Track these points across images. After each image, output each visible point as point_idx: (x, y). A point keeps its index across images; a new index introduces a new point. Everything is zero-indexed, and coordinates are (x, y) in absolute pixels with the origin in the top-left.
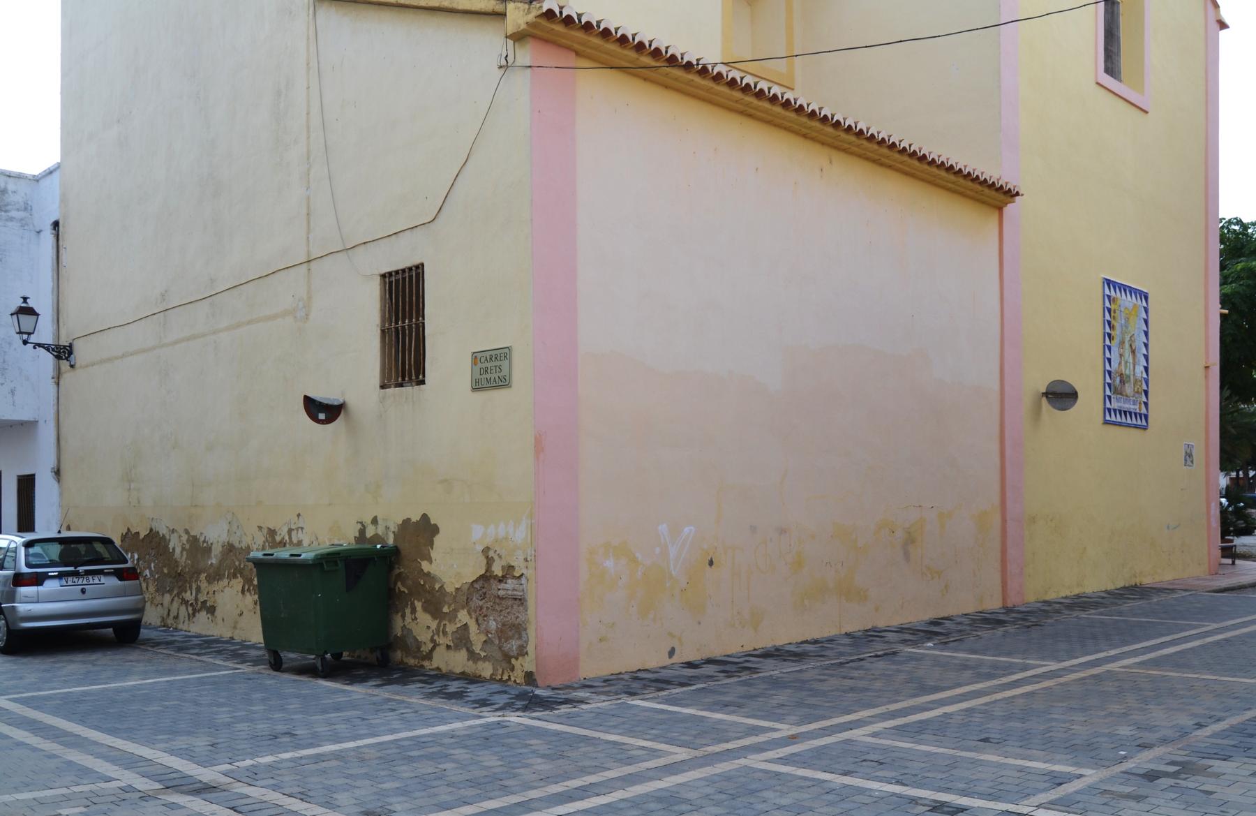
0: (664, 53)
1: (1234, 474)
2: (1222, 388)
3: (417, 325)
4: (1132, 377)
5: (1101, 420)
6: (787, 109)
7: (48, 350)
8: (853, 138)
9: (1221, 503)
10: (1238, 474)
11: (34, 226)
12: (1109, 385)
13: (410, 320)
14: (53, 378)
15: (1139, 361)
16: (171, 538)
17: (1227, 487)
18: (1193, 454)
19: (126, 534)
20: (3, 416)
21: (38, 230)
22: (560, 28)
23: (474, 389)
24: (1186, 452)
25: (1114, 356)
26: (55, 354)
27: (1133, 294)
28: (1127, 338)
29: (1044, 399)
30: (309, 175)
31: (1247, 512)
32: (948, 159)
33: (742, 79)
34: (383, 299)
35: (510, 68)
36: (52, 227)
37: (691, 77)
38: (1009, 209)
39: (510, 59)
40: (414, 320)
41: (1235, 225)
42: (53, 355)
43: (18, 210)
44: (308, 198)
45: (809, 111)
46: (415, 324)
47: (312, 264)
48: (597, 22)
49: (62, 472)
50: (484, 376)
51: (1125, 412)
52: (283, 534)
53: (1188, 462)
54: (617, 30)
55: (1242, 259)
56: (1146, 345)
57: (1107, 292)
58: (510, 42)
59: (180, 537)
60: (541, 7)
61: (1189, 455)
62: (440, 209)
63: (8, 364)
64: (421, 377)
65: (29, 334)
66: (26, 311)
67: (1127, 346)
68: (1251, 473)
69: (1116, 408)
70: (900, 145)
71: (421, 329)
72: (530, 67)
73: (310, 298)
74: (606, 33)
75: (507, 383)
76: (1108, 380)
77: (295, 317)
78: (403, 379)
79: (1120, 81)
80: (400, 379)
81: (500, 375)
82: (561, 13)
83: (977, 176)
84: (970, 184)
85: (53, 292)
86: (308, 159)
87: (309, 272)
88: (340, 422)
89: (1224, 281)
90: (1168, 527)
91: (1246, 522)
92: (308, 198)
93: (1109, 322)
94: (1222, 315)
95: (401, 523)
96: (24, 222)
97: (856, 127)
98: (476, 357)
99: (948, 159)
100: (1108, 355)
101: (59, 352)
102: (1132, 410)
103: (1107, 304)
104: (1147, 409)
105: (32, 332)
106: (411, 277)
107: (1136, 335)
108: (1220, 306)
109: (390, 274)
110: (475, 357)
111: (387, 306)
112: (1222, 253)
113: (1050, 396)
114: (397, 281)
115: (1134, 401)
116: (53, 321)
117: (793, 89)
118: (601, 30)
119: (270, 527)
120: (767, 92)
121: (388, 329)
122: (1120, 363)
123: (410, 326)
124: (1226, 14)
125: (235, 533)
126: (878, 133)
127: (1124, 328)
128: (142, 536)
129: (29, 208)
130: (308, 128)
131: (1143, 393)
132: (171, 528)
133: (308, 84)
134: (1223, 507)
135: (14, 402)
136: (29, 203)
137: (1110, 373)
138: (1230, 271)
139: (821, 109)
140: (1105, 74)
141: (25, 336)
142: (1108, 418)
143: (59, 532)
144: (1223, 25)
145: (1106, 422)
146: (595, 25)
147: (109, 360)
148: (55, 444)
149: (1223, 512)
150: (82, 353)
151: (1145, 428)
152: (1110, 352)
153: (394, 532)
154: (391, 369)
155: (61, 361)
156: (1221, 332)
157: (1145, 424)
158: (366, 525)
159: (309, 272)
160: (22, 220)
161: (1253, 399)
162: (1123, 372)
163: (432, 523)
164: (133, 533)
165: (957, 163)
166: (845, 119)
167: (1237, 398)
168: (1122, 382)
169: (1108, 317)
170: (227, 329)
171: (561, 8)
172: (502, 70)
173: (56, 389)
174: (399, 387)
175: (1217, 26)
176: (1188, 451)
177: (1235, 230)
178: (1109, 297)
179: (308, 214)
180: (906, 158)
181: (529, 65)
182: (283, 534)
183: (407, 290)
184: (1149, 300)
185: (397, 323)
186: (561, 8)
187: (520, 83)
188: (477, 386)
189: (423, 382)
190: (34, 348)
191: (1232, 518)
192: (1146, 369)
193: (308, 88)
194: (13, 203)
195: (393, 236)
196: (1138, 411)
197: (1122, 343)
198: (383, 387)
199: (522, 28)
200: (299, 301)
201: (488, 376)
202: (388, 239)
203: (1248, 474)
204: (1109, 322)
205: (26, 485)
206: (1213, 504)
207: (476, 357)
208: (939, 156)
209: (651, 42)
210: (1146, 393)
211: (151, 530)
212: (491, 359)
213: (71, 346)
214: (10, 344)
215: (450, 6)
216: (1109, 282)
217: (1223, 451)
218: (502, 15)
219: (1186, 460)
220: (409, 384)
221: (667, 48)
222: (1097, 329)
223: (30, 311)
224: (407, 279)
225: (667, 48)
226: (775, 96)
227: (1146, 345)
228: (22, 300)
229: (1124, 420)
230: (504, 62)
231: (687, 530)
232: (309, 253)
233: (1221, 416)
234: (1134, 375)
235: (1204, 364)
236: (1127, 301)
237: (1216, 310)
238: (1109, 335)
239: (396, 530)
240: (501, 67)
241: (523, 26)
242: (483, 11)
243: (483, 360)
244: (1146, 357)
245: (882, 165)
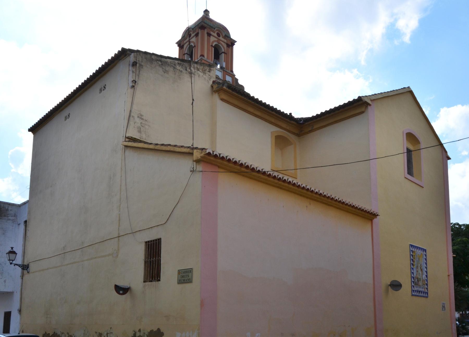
0: (292, 182)
1: (461, 313)
2: (455, 282)
3: (158, 260)
4: (421, 279)
5: (411, 295)
6: (308, 191)
7: (19, 266)
8: (318, 196)
9: (456, 324)
10: (463, 313)
11: (17, 222)
12: (413, 282)
13: (156, 258)
14: (21, 276)
15: (424, 273)
16: (62, 336)
17: (459, 317)
18: (445, 306)
19: (45, 334)
20: (1, 290)
21: (19, 223)
22: (212, 158)
23: (178, 283)
24: (443, 306)
25: (415, 271)
26: (22, 268)
27: (421, 250)
28: (419, 265)
29: (390, 287)
30: (120, 206)
31: (466, 327)
32: (352, 203)
33: (278, 176)
34: (146, 250)
35: (194, 172)
36: (24, 223)
37: (259, 175)
38: (375, 220)
39: (195, 169)
40: (157, 258)
41: (457, 225)
42: (21, 268)
43: (12, 216)
44: (119, 214)
45: (302, 187)
46: (157, 259)
47: (120, 238)
48: (226, 156)
49: (22, 311)
50: (182, 278)
51: (419, 291)
52: (105, 335)
53: (444, 309)
54: (233, 159)
55: (460, 237)
56: (426, 268)
57: (411, 249)
58: (195, 163)
59: (65, 335)
60: (206, 151)
61: (444, 307)
62: (168, 219)
63: (4, 271)
64: (159, 278)
65: (13, 260)
66: (12, 252)
67: (419, 268)
68: (468, 312)
69: (416, 290)
70: (335, 198)
71: (159, 261)
72: (202, 171)
73: (118, 250)
74: (229, 160)
75: (191, 281)
76: (413, 280)
77: (113, 256)
78: (152, 279)
79: (413, 177)
80: (151, 279)
81: (188, 278)
82: (213, 153)
83: (363, 209)
84: (361, 212)
85: (23, 245)
86: (120, 201)
87: (119, 241)
88: (128, 294)
89: (453, 245)
90: (437, 333)
91: (466, 331)
92: (119, 214)
93: (412, 260)
94: (453, 257)
95: (149, 331)
96: (14, 221)
97: (319, 192)
98: (179, 272)
99: (352, 203)
100: (412, 271)
101: (24, 267)
102: (422, 291)
103: (412, 253)
104: (427, 290)
105: (14, 260)
106: (156, 243)
107: (422, 264)
108: (452, 254)
109: (149, 242)
110: (179, 272)
111: (147, 253)
112: (452, 235)
113: (391, 286)
114: (151, 244)
115: (422, 287)
116: (22, 256)
117: (296, 178)
118: (227, 159)
119: (100, 332)
120: (287, 180)
121: (147, 261)
122: (417, 274)
123: (155, 260)
124: (449, 154)
125: (86, 334)
126: (327, 194)
127: (418, 262)
128: (51, 335)
129: (16, 216)
130: (121, 190)
131: (426, 285)
132: (62, 332)
133: (121, 175)
134: (457, 325)
135: (5, 285)
136: (16, 214)
137: (413, 277)
138: (456, 241)
139: (306, 186)
140: (408, 175)
141: (11, 261)
142: (413, 293)
143: (19, 333)
144: (449, 158)
145: (413, 295)
146: (225, 157)
147: (43, 270)
148: (20, 300)
149: (458, 327)
150: (32, 267)
151: (427, 297)
152: (413, 270)
153: (147, 335)
154: (148, 275)
155: (24, 270)
156: (453, 263)
157: (427, 296)
158: (136, 332)
159: (119, 241)
160: (13, 220)
161: (466, 286)
162: (418, 277)
163: (161, 331)
164: (47, 333)
165: (355, 205)
166: (315, 190)
167: (461, 286)
168: (418, 281)
169: (412, 258)
170: (87, 260)
171: (213, 152)
172: (191, 173)
173: (21, 280)
174: (150, 282)
175: (447, 159)
176: (443, 305)
177: (457, 227)
178: (412, 251)
179: (119, 220)
180: (337, 203)
181: (201, 170)
182: (105, 335)
183: (155, 248)
184: (427, 252)
185: (150, 259)
186: (213, 152)
187: (198, 177)
188: (180, 282)
189: (159, 280)
190: (14, 265)
191: (461, 329)
192: (427, 276)
193: (121, 177)
194: (10, 214)
195: (150, 229)
196: (424, 291)
197: (417, 267)
198: (144, 282)
199: (199, 158)
200: (115, 251)
201: (184, 279)
202: (148, 230)
203: (466, 313)
204: (412, 260)
205: (8, 316)
206: (453, 325)
207: (179, 272)
208: (349, 202)
209: (245, 163)
210: (427, 285)
211: (54, 333)
212: (185, 272)
213: (28, 265)
214: (5, 264)
215: (173, 150)
216: (412, 246)
217: (456, 305)
218: (192, 154)
219: (442, 309)
220: (154, 281)
221: (251, 165)
222: (408, 262)
223: (14, 253)
224: (155, 243)
225: (251, 165)
226: (290, 182)
227: (426, 268)
228: (11, 248)
229: (419, 294)
230: (192, 170)
231: (257, 334)
232: (119, 234)
233: (455, 292)
234: (422, 278)
235: (447, 274)
236: (419, 252)
237: (451, 255)
238: (413, 264)
239: (148, 334)
240: (191, 171)
241: (199, 158)
242: (185, 152)
243: (182, 273)
244: (426, 272)
245: (329, 205)
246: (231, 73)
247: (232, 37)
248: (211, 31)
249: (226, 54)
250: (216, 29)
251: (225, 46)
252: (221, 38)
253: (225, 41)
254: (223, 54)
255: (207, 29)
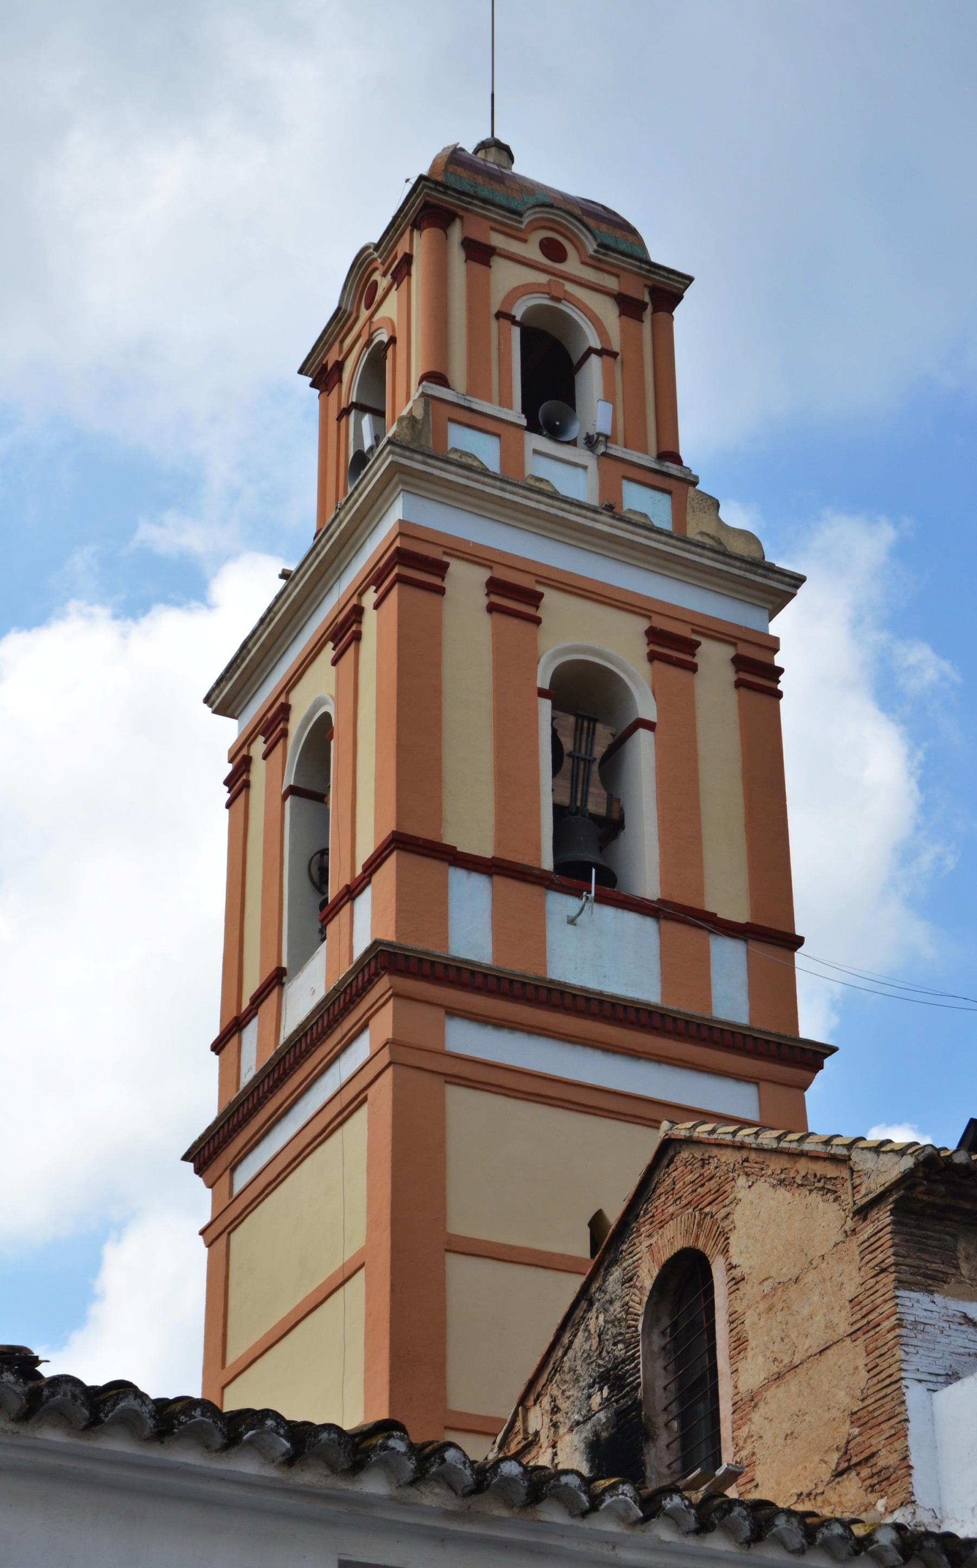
245: (504, 506)
246: (672, 468)
247: (658, 254)
248: (493, 229)
249: (614, 355)
250: (526, 220)
251: (608, 312)
252: (572, 265)
253: (611, 283)
254: (594, 360)
255: (462, 226)
